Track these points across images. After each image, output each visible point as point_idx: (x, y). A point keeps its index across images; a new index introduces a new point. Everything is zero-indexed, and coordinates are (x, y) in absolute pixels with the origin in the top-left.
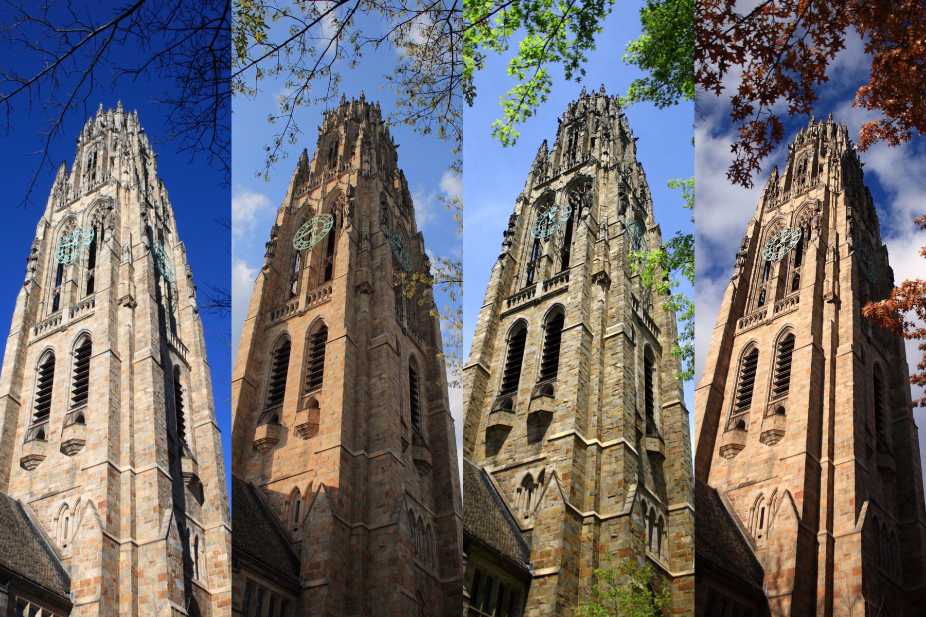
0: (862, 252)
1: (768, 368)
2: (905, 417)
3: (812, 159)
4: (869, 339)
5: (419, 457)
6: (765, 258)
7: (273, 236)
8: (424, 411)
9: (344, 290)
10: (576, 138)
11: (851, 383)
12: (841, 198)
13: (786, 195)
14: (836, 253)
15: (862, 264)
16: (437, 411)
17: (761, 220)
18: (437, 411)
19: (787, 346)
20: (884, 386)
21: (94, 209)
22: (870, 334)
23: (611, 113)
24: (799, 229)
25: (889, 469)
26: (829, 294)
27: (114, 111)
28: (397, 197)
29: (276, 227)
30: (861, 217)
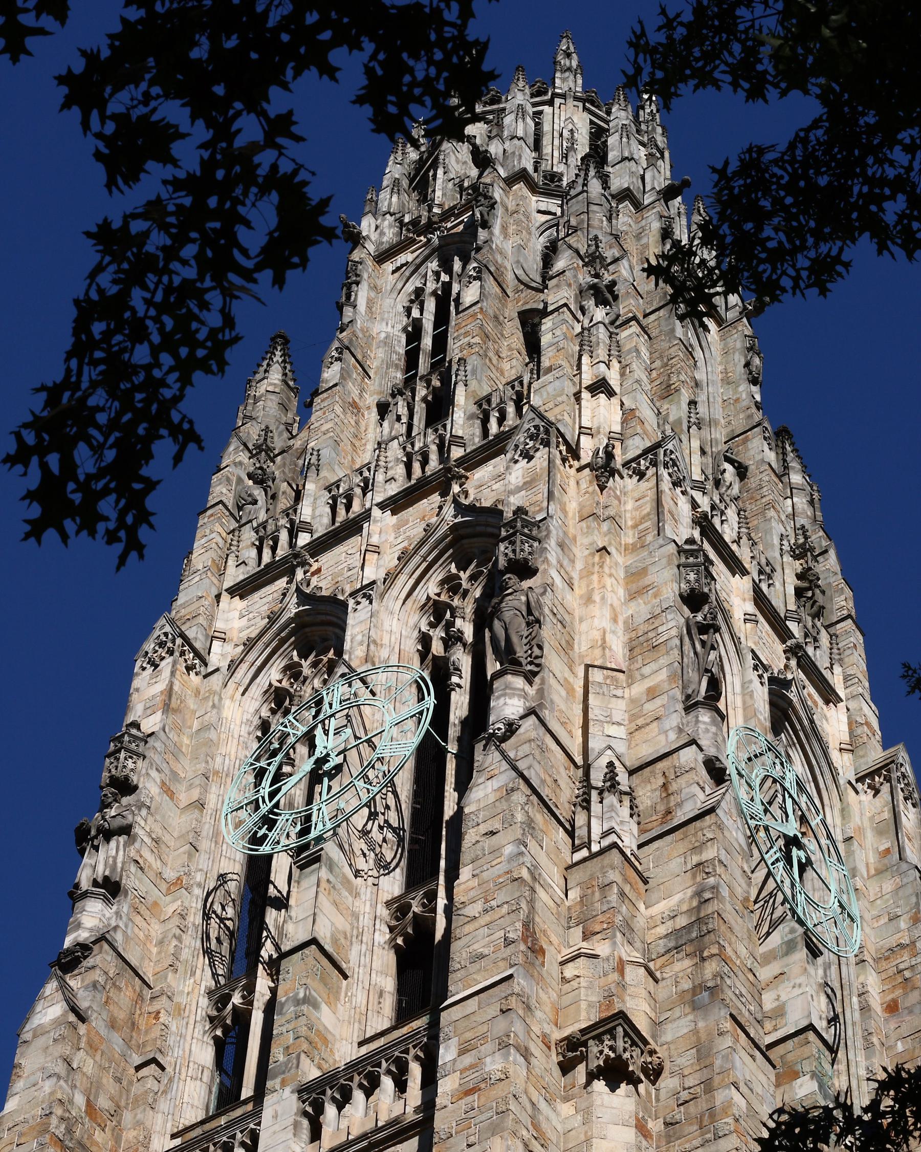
10: (442, 318)
21: (437, 576)
23: (618, 182)
27: (543, 91)
28: (767, 572)
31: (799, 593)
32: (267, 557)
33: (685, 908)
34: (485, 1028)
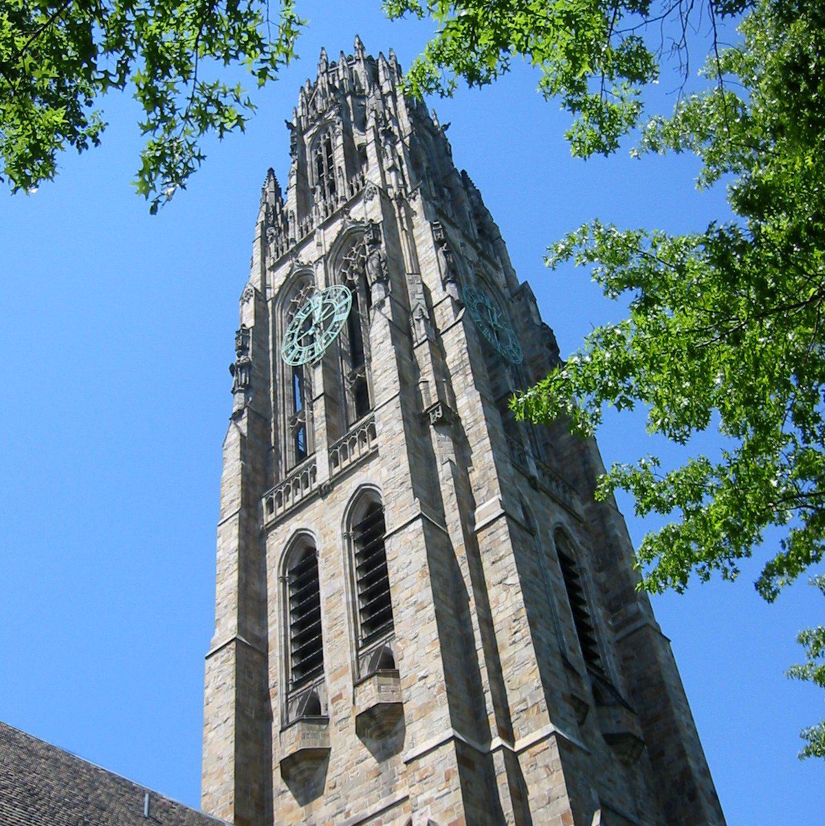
0: (482, 307)
1: (341, 582)
2: (638, 624)
3: (340, 141)
4: (532, 482)
5: (613, 728)
6: (288, 361)
7: (242, 350)
8: (605, 635)
9: (399, 426)
11: (514, 579)
12: (416, 205)
13: (306, 220)
14: (431, 322)
15: (486, 332)
16: (631, 628)
17: (265, 286)
18: (631, 628)
19: (368, 526)
20: (582, 570)
22: (533, 471)
24: (344, 288)
25: (630, 735)
26: (434, 408)
28: (466, 226)
29: (243, 333)
30: (465, 236)
31: (479, 231)
32: (281, 255)
33: (456, 358)
34: (391, 415)
